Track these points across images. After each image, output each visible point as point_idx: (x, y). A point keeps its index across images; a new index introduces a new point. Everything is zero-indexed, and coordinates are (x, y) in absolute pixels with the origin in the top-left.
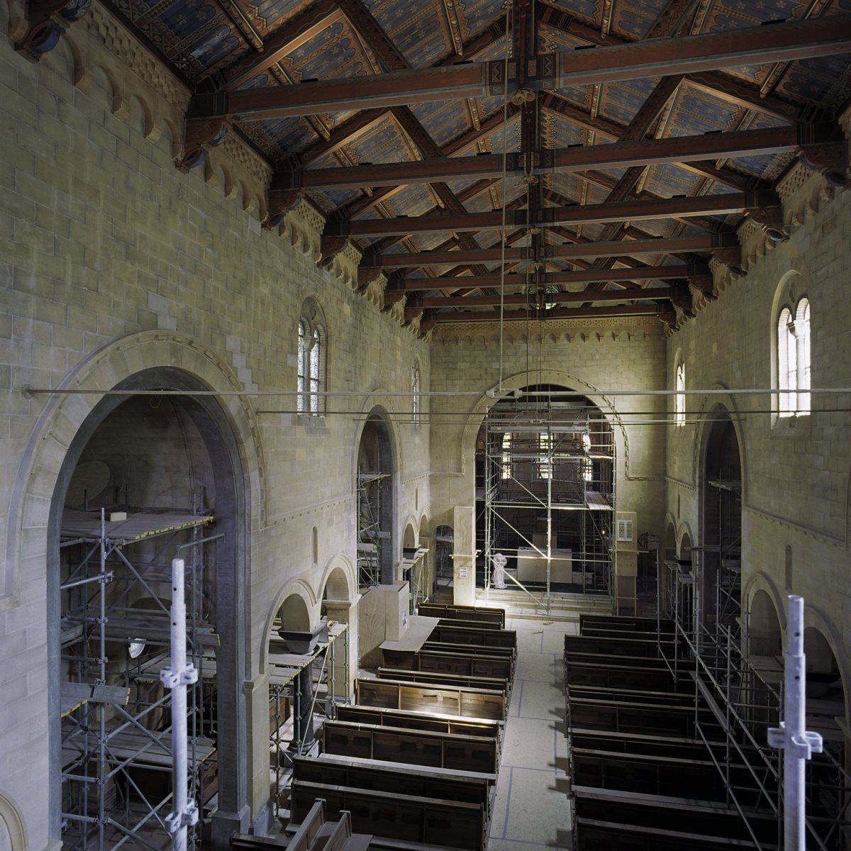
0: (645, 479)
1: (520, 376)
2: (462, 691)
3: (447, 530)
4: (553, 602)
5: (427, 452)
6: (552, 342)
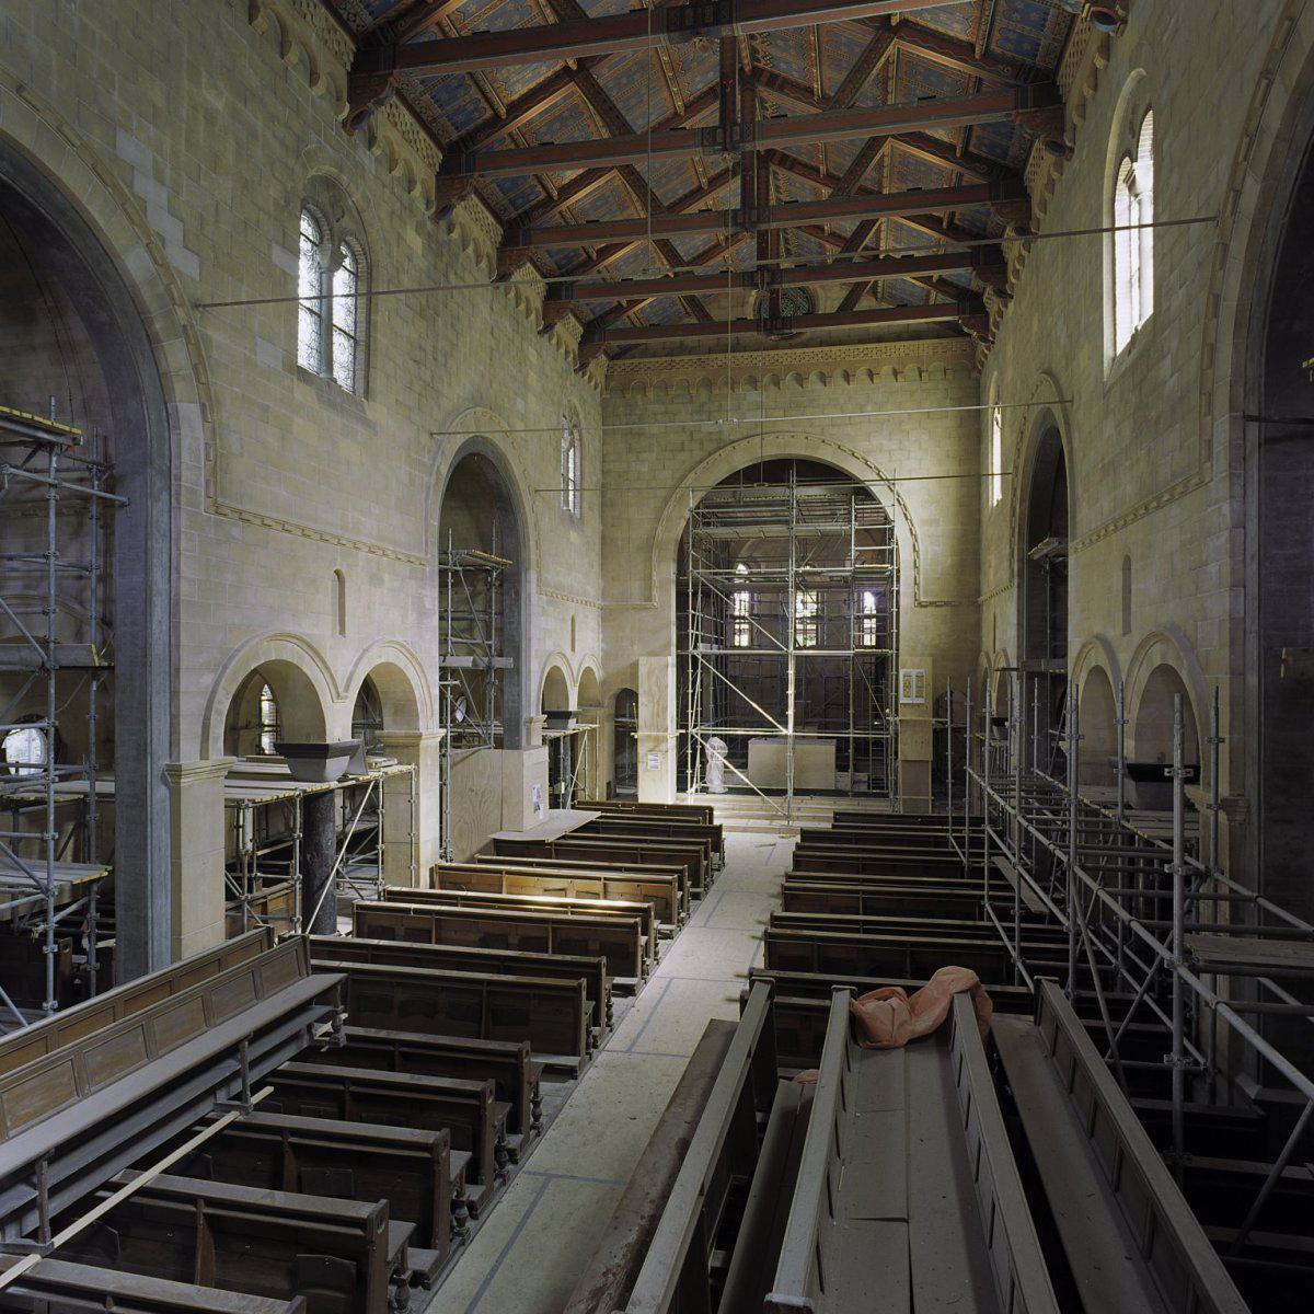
0: (946, 604)
1: (745, 442)
2: (605, 879)
3: (626, 700)
4: (799, 809)
5: (597, 568)
6: (797, 386)
